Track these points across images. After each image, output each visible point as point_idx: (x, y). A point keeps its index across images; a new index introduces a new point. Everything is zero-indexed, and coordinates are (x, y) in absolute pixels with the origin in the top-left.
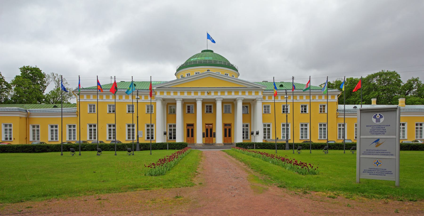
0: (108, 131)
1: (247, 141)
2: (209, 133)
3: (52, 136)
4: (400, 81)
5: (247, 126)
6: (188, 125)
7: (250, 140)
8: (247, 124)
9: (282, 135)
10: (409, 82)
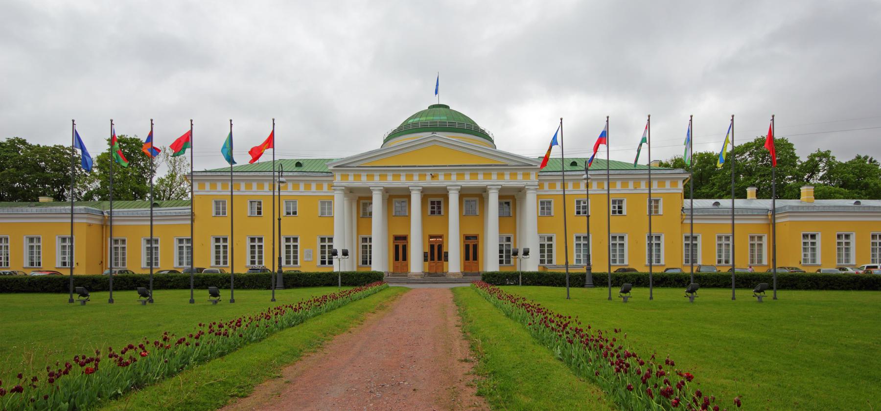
0: (249, 250)
1: (507, 269)
2: (436, 253)
3: (253, 257)
4: (794, 157)
5: (508, 239)
6: (397, 238)
7: (514, 266)
8: (508, 235)
9: (575, 258)
10: (812, 158)
